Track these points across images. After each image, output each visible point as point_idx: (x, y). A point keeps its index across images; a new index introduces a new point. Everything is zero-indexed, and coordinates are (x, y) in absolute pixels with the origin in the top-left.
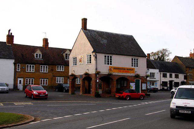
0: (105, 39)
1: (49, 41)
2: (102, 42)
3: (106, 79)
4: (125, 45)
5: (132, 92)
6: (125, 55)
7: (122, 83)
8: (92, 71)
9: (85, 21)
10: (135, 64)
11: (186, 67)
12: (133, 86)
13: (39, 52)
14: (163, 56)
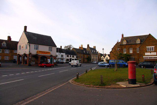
0: (36, 37)
1: (11, 38)
2: (34, 38)
3: (36, 56)
4: (47, 41)
5: (47, 64)
6: (46, 45)
7: (44, 58)
8: (27, 53)
9: (26, 27)
10: (50, 50)
11: (77, 53)
12: (49, 61)
13: (4, 43)
14: (70, 48)
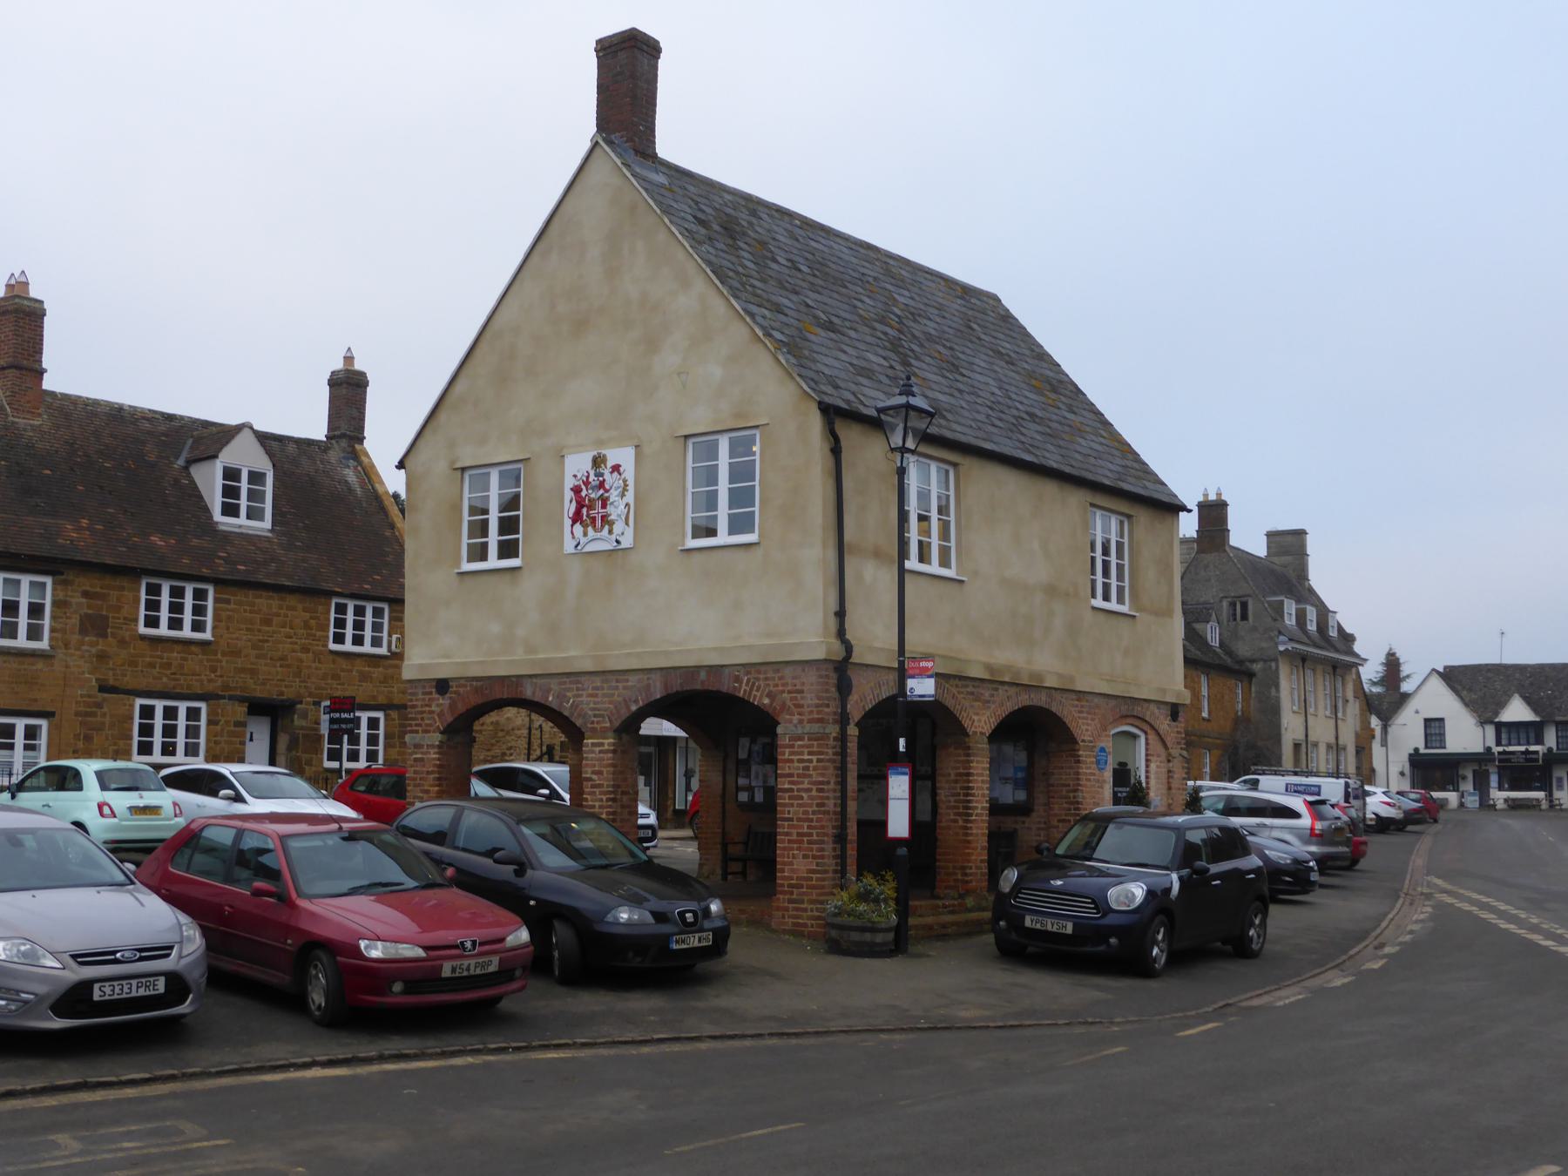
9: (628, 67)
